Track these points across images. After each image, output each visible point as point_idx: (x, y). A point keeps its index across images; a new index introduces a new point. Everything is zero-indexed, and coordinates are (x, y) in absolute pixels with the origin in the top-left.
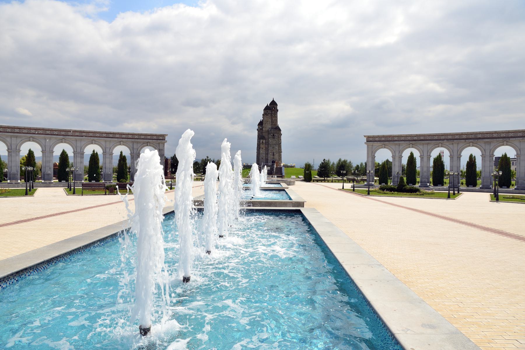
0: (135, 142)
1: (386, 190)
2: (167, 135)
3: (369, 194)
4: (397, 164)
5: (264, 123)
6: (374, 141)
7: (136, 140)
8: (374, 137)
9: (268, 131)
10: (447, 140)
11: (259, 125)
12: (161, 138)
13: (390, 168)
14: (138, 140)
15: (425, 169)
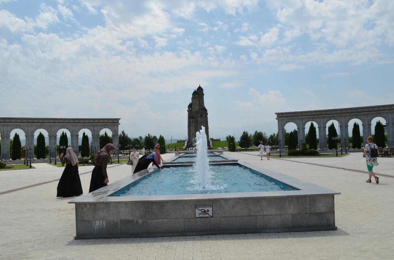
0: (96, 125)
1: (293, 154)
2: (120, 119)
3: (280, 157)
4: (301, 134)
5: (193, 105)
6: (283, 118)
7: (96, 124)
8: (282, 114)
9: (197, 111)
10: (337, 114)
11: (189, 107)
12: (115, 121)
13: (297, 138)
14: (98, 124)
15: (323, 137)
